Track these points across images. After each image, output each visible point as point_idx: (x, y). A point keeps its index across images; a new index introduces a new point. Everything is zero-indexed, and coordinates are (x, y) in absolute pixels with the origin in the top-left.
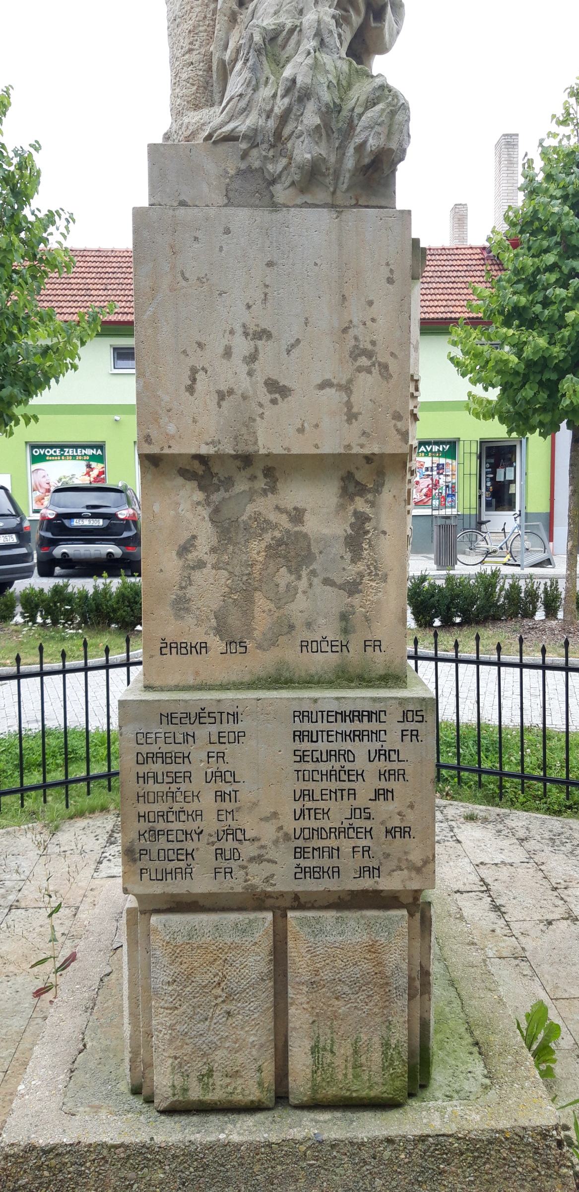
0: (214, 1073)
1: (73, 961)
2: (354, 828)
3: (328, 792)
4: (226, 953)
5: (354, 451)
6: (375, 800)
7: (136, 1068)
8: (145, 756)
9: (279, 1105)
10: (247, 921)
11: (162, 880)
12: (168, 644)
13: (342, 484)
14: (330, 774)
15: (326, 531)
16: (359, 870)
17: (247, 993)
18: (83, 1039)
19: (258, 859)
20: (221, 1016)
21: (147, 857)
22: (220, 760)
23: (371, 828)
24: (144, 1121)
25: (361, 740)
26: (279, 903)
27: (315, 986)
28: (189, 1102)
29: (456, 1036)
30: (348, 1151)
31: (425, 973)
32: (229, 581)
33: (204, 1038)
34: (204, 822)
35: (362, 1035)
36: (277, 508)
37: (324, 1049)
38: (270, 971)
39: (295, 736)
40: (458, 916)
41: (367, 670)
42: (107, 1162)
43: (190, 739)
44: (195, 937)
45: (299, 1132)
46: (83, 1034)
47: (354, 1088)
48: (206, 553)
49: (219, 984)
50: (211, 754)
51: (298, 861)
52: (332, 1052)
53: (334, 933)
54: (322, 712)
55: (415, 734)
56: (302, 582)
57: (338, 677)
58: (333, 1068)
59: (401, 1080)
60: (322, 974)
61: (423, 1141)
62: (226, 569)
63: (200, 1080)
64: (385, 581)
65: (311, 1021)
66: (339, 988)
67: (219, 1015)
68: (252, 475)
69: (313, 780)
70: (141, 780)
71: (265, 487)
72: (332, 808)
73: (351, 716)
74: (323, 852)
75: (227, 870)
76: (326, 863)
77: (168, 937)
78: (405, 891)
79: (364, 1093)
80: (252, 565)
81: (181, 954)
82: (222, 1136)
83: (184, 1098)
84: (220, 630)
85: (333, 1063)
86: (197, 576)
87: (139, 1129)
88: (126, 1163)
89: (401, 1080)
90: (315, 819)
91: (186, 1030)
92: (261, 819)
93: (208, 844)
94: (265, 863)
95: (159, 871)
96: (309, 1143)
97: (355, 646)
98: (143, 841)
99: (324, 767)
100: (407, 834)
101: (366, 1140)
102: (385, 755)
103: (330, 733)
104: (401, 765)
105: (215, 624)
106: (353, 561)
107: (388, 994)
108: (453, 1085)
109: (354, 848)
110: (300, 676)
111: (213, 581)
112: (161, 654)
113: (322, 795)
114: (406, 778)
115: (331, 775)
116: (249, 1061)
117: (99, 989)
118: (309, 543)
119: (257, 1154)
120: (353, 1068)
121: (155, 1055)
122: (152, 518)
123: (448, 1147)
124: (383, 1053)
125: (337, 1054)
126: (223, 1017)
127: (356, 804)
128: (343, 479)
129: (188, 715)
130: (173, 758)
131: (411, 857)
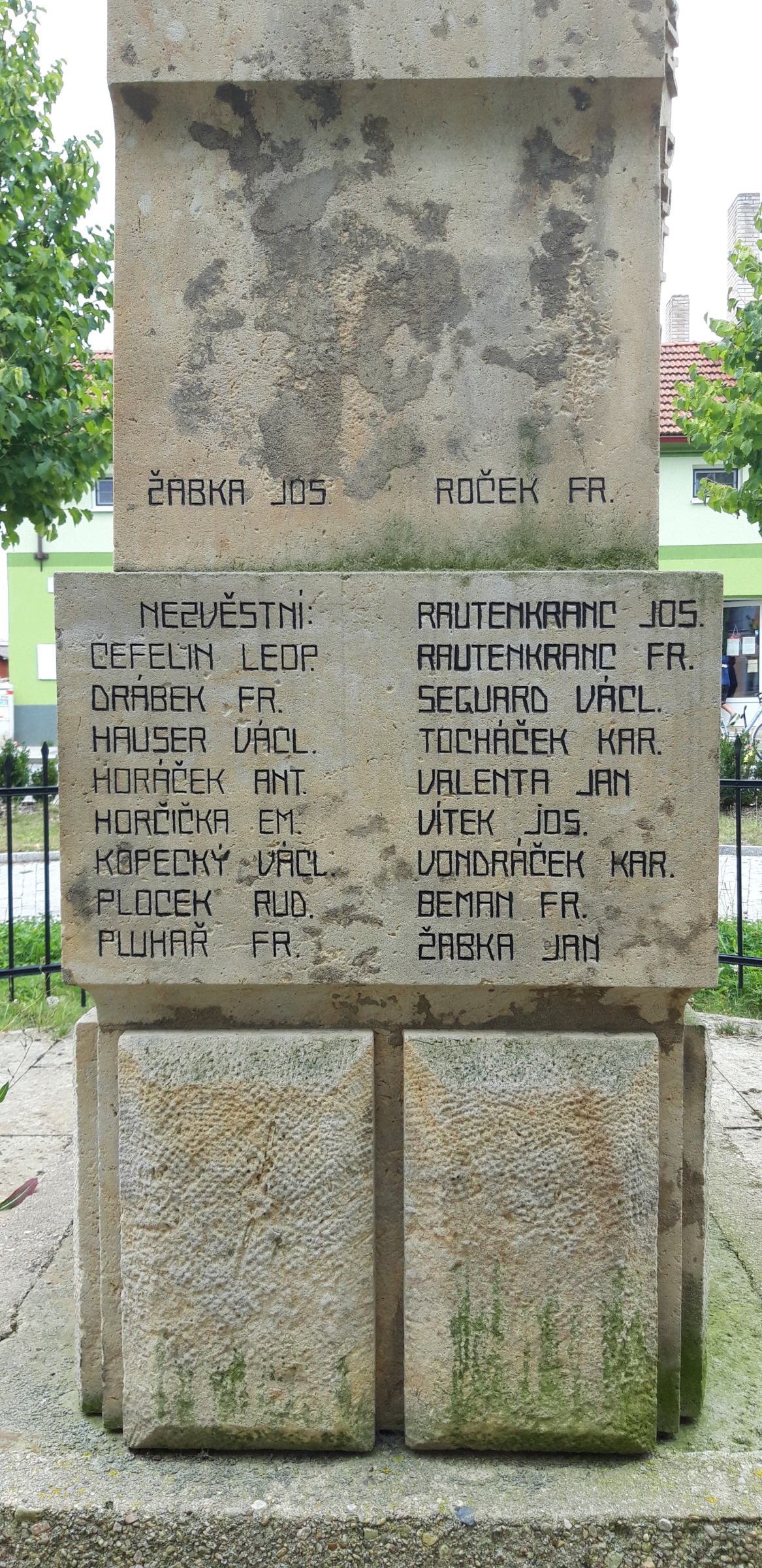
0: (247, 1371)
1: (30, 1193)
2: (543, 853)
3: (490, 776)
4: (273, 1110)
5: (550, 73)
6: (590, 793)
7: (93, 1360)
8: (110, 693)
9: (385, 1446)
10: (319, 1045)
11: (144, 955)
12: (166, 482)
13: (525, 154)
14: (493, 738)
15: (490, 251)
16: (554, 942)
17: (317, 1199)
18: (15, 1316)
19: (343, 915)
20: (262, 1246)
21: (114, 906)
22: (266, 704)
23: (581, 854)
24: (98, 1468)
25: (562, 666)
26: (392, 1014)
27: (460, 1187)
28: (192, 1431)
29: (746, 1333)
30: (530, 1548)
31: (693, 1179)
32: (289, 355)
33: (225, 1295)
34: (231, 835)
35: (561, 1298)
36: (392, 204)
37: (480, 1326)
38: (365, 1154)
39: (420, 655)
40: (727, 1145)
41: (575, 540)
42: (11, 1550)
43: (204, 658)
44: (209, 1074)
45: (425, 1503)
46: (17, 1306)
47: (543, 1413)
48: (244, 297)
49: (258, 1177)
50: (246, 693)
51: (426, 921)
52: (496, 1333)
53: (500, 1074)
54: (479, 604)
55: (677, 653)
56: (441, 356)
57: (514, 555)
58: (498, 1368)
59: (643, 1400)
60: (476, 1162)
61: (694, 1531)
62: (284, 330)
63: (217, 1385)
64: (614, 355)
65: (451, 1264)
66: (511, 1192)
67: (258, 1244)
68: (340, 136)
69: (459, 751)
70: (102, 744)
71: (365, 161)
72: (498, 809)
73: (541, 614)
74: (479, 902)
75: (279, 937)
76: (485, 926)
77: (152, 1073)
78: (653, 990)
79: (564, 1425)
80: (338, 322)
81: (179, 1109)
82: (258, 1505)
83: (183, 1422)
84: (270, 457)
85: (498, 1357)
86: (225, 342)
87: (86, 1482)
88: (52, 1554)
89: (643, 1400)
90: (463, 832)
91: (188, 1275)
92: (350, 832)
93: (240, 881)
94: (356, 924)
95: (139, 935)
96: (445, 1528)
97: (551, 488)
98: (104, 872)
99: (482, 722)
100: (657, 868)
101: (568, 1525)
102: (612, 697)
103: (495, 651)
104: (646, 720)
105: (261, 444)
106: (548, 312)
107: (618, 1209)
108: (750, 1421)
109: (543, 894)
110: (434, 553)
111: (257, 355)
112: (151, 503)
113: (477, 781)
114: (657, 748)
115: (496, 740)
116: (319, 1345)
117: (65, 1236)
118: (457, 275)
119: (332, 1548)
120: (541, 1370)
121: (126, 1327)
122: (137, 226)
123: (749, 1546)
124: (605, 1339)
125: (507, 1337)
126: (267, 1248)
127: (548, 802)
128: (526, 144)
129: (198, 608)
130: (168, 699)
131: (666, 917)
